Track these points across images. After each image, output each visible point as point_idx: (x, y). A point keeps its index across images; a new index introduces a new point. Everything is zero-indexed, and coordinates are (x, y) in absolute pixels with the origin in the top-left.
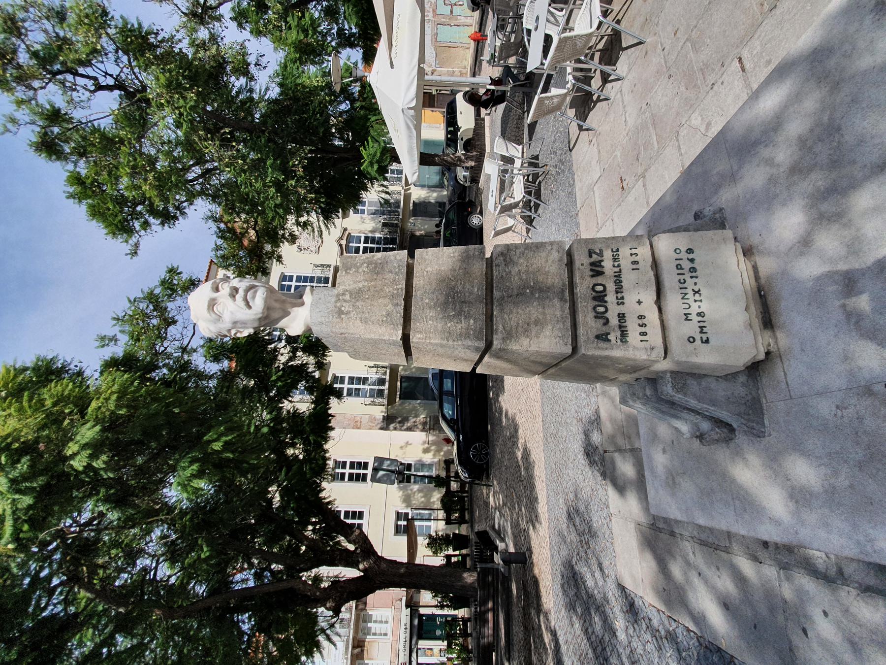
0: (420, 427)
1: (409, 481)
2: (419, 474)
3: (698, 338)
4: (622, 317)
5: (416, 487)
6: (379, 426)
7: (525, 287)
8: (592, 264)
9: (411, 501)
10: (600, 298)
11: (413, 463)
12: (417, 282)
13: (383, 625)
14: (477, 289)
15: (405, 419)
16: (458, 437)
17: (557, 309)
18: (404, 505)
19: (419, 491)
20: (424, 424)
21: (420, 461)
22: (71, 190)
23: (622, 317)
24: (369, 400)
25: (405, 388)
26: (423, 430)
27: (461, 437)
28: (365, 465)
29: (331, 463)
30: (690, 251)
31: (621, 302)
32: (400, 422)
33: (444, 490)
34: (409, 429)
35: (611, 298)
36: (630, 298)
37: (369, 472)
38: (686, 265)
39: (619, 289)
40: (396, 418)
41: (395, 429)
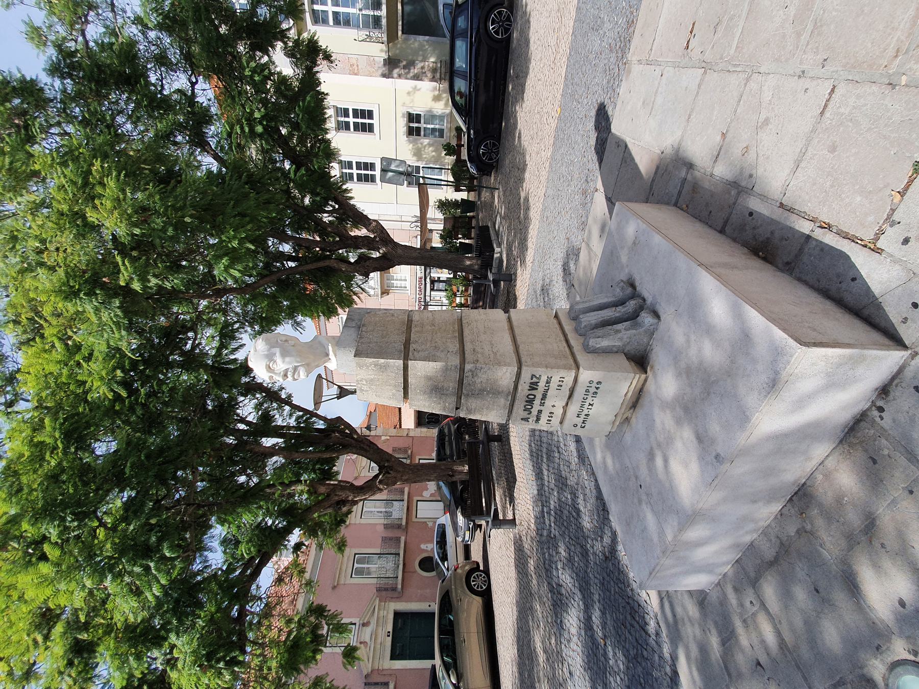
0: (429, 75)
1: (418, 134)
2: (429, 126)
3: (579, 426)
4: (540, 412)
5: (426, 141)
6: (380, 72)
7: (484, 390)
8: (531, 383)
9: (421, 155)
10: (530, 401)
11: (422, 114)
12: (411, 380)
13: (403, 282)
14: (452, 385)
15: (411, 64)
16: (468, 129)
17: (503, 401)
18: (415, 158)
19: (430, 145)
20: (434, 70)
21: (430, 111)
22: (315, 604)
23: (540, 412)
24: (363, 33)
25: (409, 14)
26: (433, 79)
27: (472, 132)
28: (372, 166)
29: (330, 112)
30: (599, 383)
31: (542, 404)
32: (405, 67)
33: (453, 158)
34: (417, 77)
35: (537, 402)
36: (549, 402)
37: (377, 173)
38: (593, 390)
39: (544, 397)
40: (399, 61)
41: (400, 76)
